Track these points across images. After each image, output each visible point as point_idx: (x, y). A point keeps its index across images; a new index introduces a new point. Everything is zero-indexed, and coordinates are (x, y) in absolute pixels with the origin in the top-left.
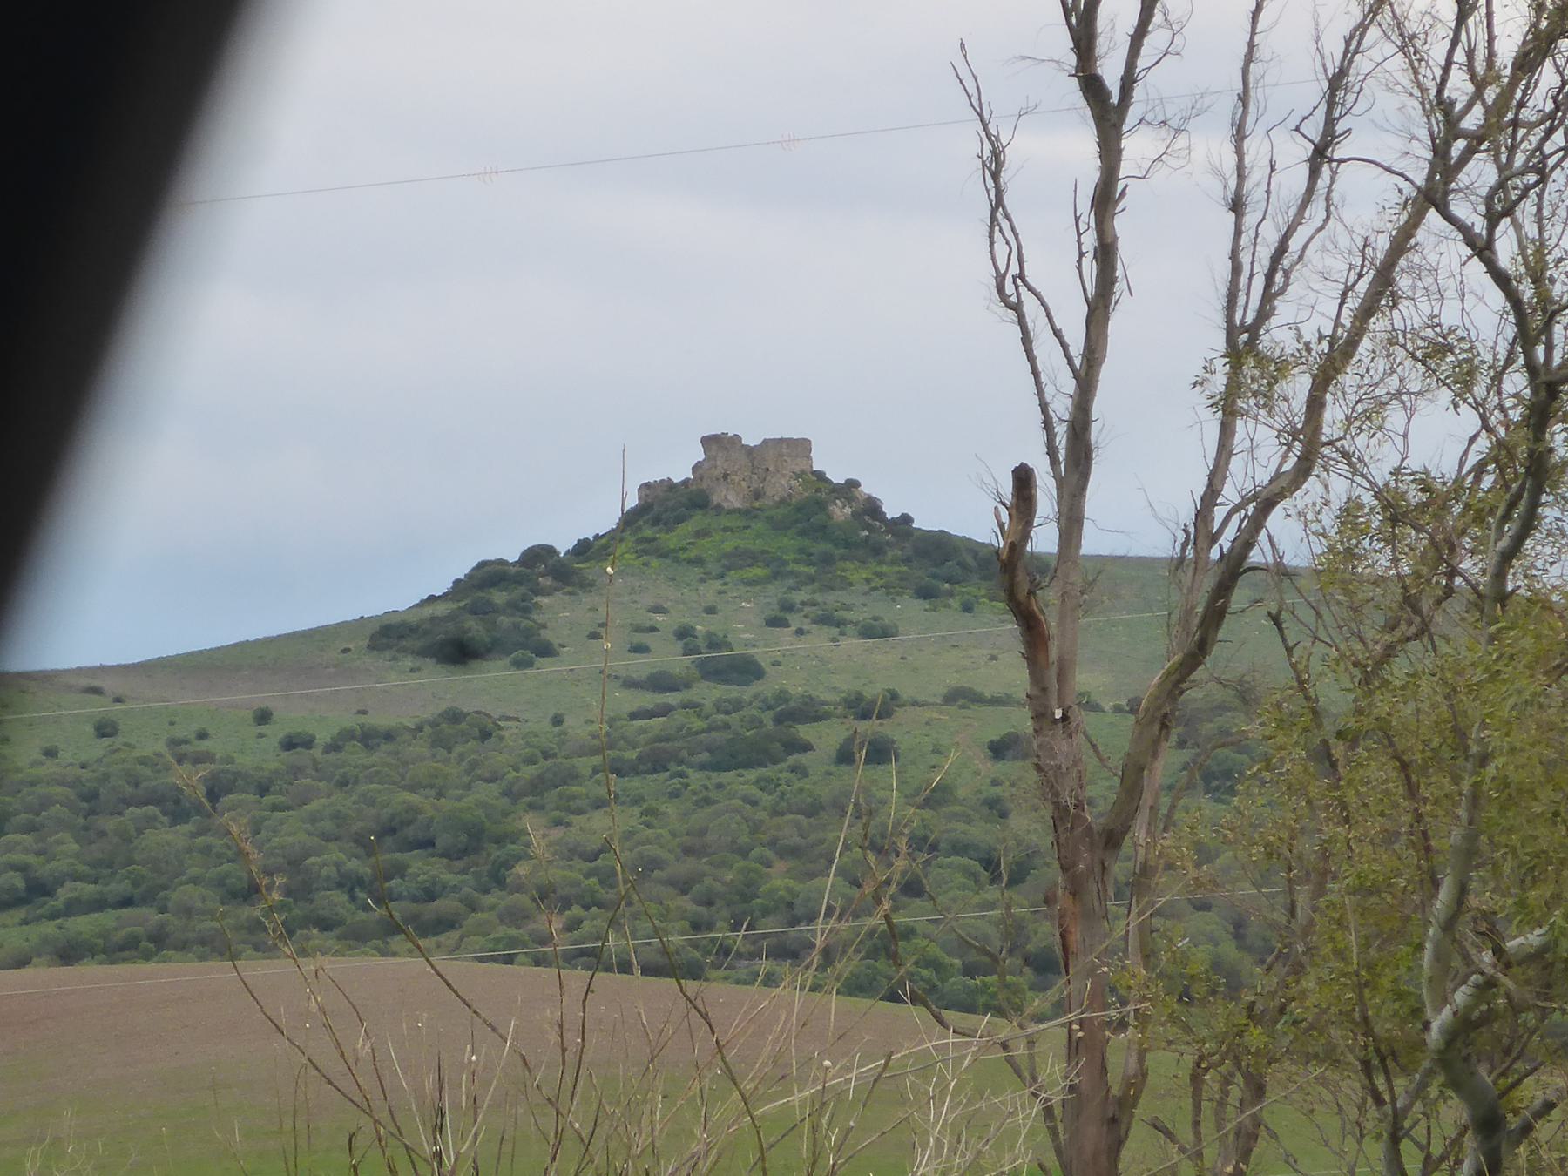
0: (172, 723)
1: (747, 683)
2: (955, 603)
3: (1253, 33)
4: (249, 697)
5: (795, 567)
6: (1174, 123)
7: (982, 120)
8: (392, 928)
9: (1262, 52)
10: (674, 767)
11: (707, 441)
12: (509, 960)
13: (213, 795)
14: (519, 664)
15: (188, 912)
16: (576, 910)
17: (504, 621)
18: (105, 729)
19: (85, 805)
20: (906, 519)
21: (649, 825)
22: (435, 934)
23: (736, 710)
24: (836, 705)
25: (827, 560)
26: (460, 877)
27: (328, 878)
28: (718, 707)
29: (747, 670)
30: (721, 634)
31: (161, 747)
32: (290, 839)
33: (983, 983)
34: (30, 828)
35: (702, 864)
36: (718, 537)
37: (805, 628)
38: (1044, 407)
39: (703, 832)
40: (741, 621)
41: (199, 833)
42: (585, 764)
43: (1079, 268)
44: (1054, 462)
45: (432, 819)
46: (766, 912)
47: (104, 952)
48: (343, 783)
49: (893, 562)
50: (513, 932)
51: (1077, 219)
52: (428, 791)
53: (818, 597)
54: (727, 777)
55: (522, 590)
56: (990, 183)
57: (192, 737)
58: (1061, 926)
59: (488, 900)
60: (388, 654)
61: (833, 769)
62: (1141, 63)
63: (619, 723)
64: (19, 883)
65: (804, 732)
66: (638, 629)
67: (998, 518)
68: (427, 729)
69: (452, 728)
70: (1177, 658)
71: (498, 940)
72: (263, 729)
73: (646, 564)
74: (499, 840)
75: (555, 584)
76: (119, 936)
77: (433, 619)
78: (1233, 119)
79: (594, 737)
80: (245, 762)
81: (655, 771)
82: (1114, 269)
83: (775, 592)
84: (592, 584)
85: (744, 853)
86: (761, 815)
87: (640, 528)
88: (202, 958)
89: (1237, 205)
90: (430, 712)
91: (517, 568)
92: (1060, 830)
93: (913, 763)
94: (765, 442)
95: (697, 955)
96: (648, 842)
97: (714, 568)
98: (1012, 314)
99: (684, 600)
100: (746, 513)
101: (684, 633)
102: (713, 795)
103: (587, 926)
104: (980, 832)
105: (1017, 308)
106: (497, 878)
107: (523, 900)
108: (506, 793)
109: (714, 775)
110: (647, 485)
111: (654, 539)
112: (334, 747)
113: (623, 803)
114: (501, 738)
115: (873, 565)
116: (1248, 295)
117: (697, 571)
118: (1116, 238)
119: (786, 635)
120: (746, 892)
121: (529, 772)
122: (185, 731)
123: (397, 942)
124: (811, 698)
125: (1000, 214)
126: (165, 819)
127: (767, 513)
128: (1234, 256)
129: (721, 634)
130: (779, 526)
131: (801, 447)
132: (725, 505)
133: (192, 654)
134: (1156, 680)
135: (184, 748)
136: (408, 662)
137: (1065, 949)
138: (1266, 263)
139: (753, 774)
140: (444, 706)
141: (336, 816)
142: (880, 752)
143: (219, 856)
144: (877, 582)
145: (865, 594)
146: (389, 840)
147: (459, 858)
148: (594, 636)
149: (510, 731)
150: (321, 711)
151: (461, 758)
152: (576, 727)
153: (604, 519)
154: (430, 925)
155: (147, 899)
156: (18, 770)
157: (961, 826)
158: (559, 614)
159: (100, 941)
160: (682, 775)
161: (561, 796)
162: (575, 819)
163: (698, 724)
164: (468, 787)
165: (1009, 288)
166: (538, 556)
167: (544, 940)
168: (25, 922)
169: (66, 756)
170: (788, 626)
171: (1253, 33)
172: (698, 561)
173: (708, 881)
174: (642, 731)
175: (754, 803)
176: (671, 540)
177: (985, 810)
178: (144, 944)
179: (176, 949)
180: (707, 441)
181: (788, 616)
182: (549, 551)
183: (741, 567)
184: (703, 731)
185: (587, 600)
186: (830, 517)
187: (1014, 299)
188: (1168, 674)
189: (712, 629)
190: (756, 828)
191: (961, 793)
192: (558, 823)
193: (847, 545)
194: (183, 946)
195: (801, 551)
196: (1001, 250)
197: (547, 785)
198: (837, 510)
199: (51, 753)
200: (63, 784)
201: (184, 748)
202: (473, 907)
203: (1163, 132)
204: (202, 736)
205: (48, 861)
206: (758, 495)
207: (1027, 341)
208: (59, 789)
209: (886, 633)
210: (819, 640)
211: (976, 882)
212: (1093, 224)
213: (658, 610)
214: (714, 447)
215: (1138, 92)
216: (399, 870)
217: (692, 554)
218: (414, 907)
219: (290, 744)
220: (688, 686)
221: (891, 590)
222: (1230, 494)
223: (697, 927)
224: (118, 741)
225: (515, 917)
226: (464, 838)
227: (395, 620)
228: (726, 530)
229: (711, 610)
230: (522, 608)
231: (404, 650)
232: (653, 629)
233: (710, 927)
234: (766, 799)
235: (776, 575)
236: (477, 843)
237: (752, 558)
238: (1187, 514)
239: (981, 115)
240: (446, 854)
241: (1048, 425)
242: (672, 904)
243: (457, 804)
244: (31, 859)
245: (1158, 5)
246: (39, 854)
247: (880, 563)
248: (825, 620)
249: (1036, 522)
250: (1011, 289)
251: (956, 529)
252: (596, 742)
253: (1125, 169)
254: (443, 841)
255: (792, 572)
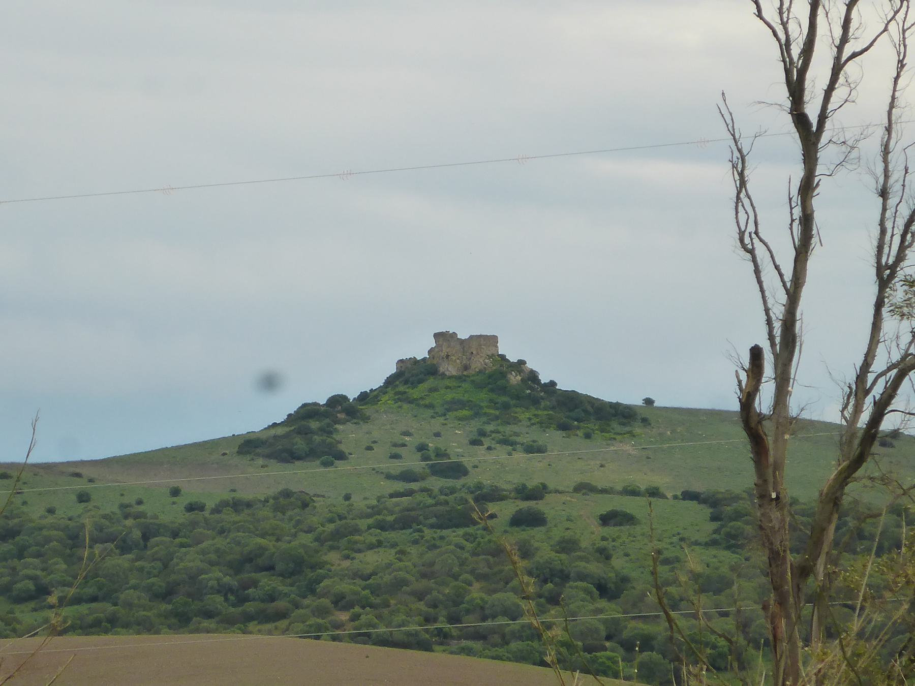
0: (122, 495)
1: (458, 478)
2: (580, 433)
3: (894, 91)
4: (165, 480)
5: (488, 411)
6: (850, 143)
7: (734, 139)
8: (249, 618)
9: (901, 102)
10: (415, 526)
11: (437, 336)
12: (318, 638)
13: (146, 537)
14: (326, 464)
15: (129, 605)
16: (357, 609)
17: (317, 438)
18: (83, 498)
19: (70, 542)
20: (553, 384)
21: (400, 560)
22: (274, 622)
23: (452, 493)
24: (510, 492)
25: (506, 407)
26: (290, 588)
27: (212, 588)
28: (441, 491)
29: (458, 470)
30: (443, 449)
31: (115, 509)
32: (191, 564)
33: (596, 656)
34: (38, 555)
35: (431, 583)
36: (443, 391)
37: (493, 446)
38: (767, 311)
39: (432, 564)
40: (455, 441)
41: (137, 560)
42: (363, 524)
43: (791, 229)
44: (773, 345)
45: (274, 553)
46: (468, 612)
47: (81, 628)
48: (222, 532)
49: (545, 409)
50: (320, 621)
51: (790, 199)
52: (271, 538)
53: (501, 429)
54: (445, 532)
55: (327, 421)
56: (737, 177)
57: (133, 502)
58: (772, 623)
59: (306, 602)
60: (249, 457)
61: (508, 529)
62: (831, 107)
63: (383, 500)
64: (32, 587)
65: (492, 508)
66: (395, 445)
67: (738, 377)
68: (271, 501)
69: (286, 500)
70: (845, 464)
71: (311, 626)
72: (175, 499)
73: (400, 407)
74: (313, 567)
75: (347, 418)
76: (90, 619)
77: (275, 437)
78: (882, 141)
79: (368, 508)
80: (164, 519)
81: (404, 528)
82: (811, 230)
83: (475, 425)
84: (368, 418)
85: (456, 577)
86: (466, 555)
87: (397, 386)
88: (138, 633)
89: (884, 193)
90: (273, 491)
91: (325, 408)
92: (773, 566)
93: (555, 526)
94: (471, 337)
95: (427, 636)
96: (400, 569)
97: (439, 410)
98: (749, 256)
99: (420, 428)
100: (459, 378)
101: (422, 448)
102: (438, 543)
103: (363, 617)
104: (594, 568)
105: (751, 252)
106: (311, 589)
107: (326, 602)
108: (317, 539)
109: (439, 531)
110: (401, 361)
111: (405, 393)
112: (217, 510)
113: (385, 547)
114: (315, 507)
115: (533, 411)
116: (890, 247)
117: (430, 412)
118: (813, 212)
119: (481, 450)
120: (457, 599)
121: (331, 527)
122: (129, 499)
123: (252, 626)
124: (496, 487)
125: (742, 195)
126: (117, 551)
127: (472, 378)
128: (882, 224)
129: (443, 449)
130: (479, 386)
131: (492, 340)
132: (447, 373)
133: (134, 454)
134: (832, 477)
135: (128, 510)
136: (260, 461)
137: (775, 636)
138: (902, 228)
139: (461, 531)
140: (281, 488)
141: (217, 551)
142: (534, 520)
143: (149, 573)
144: (535, 420)
145: (528, 426)
146: (248, 566)
147: (290, 577)
148: (369, 448)
149: (319, 503)
150: (209, 488)
151: (291, 519)
152: (359, 502)
153: (377, 382)
154: (270, 616)
155: (106, 597)
156: (31, 521)
157: (583, 564)
158: (349, 435)
159: (79, 622)
160: (420, 531)
161: (349, 542)
162: (357, 555)
163: (430, 501)
164: (295, 535)
165: (747, 240)
166: (337, 401)
167: (338, 626)
168: (35, 610)
169: (60, 513)
170: (482, 445)
171: (894, 91)
172: (430, 406)
173: (435, 593)
174: (397, 505)
175: (462, 548)
176: (415, 393)
177: (598, 555)
178: (103, 624)
179: (123, 627)
180: (437, 336)
181: (483, 439)
182: (345, 398)
183: (456, 410)
184: (433, 505)
185: (365, 427)
186: (508, 381)
187: (750, 247)
188: (840, 473)
189: (439, 446)
190: (463, 563)
191: (583, 545)
192: (347, 557)
193: (518, 397)
194: (127, 626)
195: (491, 401)
196: (742, 217)
197: (341, 535)
198: (512, 378)
199: (51, 511)
200: (56, 530)
201: (128, 510)
202: (297, 606)
203: (844, 148)
204: (140, 502)
205: (49, 574)
206: (466, 368)
207: (757, 271)
208: (55, 532)
209: (540, 450)
210: (501, 454)
211: (592, 597)
212: (799, 203)
213: (406, 434)
214: (441, 339)
215: (828, 124)
216: (254, 584)
217: (427, 402)
218: (262, 606)
219: (191, 508)
220: (423, 479)
221: (544, 425)
222: (878, 365)
223: (427, 620)
224: (90, 505)
225: (322, 612)
226: (292, 565)
227: (253, 437)
228: (447, 388)
229: (437, 435)
230: (328, 431)
231: (258, 455)
232: (404, 445)
233: (435, 620)
234: (469, 546)
235: (477, 415)
236: (298, 568)
237: (462, 405)
238: (851, 377)
239: (733, 135)
240: (281, 575)
241: (769, 322)
242: (413, 606)
243: (288, 545)
244: (39, 573)
245: (842, 72)
246: (43, 570)
247: (537, 409)
248: (505, 442)
249: (763, 380)
250: (747, 243)
251: (580, 391)
252: (369, 510)
253: (819, 170)
254: (280, 567)
255: (485, 414)
